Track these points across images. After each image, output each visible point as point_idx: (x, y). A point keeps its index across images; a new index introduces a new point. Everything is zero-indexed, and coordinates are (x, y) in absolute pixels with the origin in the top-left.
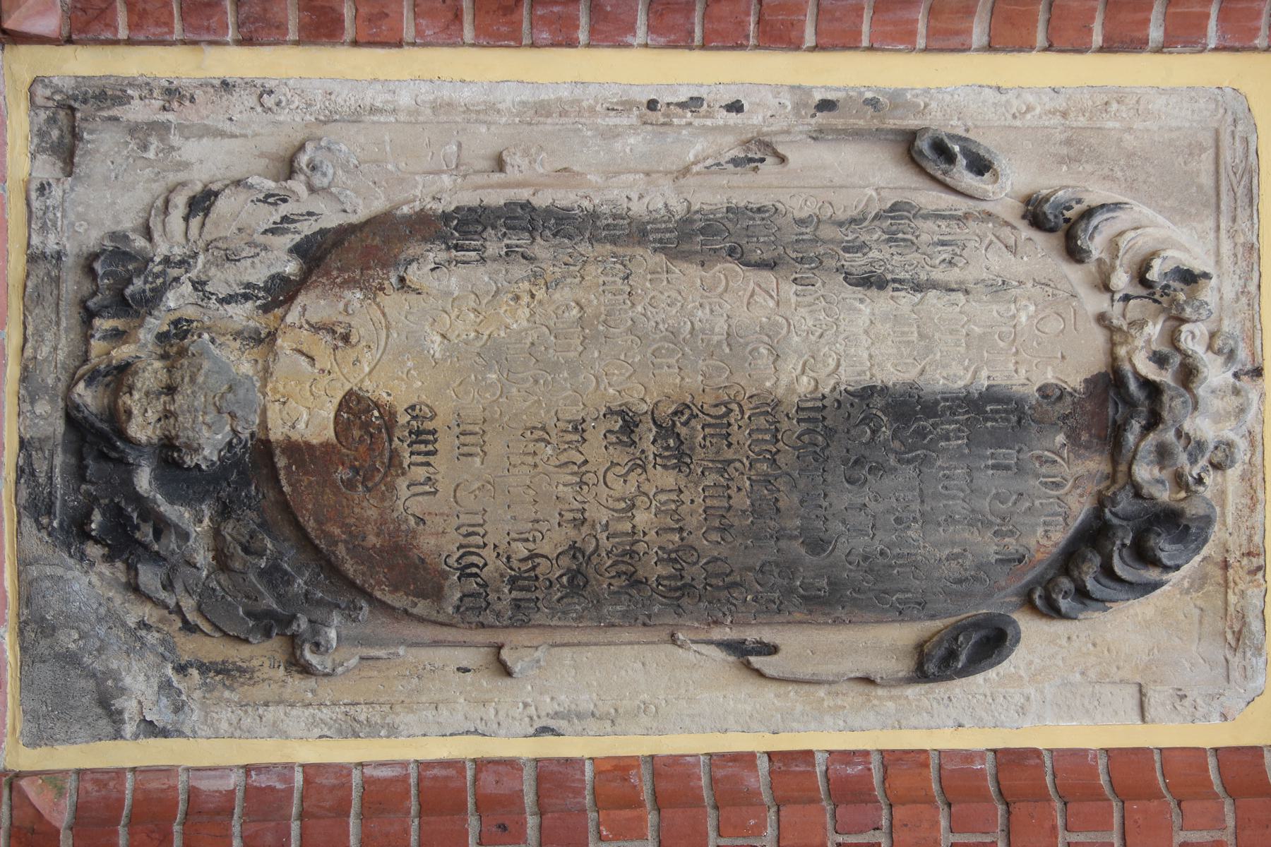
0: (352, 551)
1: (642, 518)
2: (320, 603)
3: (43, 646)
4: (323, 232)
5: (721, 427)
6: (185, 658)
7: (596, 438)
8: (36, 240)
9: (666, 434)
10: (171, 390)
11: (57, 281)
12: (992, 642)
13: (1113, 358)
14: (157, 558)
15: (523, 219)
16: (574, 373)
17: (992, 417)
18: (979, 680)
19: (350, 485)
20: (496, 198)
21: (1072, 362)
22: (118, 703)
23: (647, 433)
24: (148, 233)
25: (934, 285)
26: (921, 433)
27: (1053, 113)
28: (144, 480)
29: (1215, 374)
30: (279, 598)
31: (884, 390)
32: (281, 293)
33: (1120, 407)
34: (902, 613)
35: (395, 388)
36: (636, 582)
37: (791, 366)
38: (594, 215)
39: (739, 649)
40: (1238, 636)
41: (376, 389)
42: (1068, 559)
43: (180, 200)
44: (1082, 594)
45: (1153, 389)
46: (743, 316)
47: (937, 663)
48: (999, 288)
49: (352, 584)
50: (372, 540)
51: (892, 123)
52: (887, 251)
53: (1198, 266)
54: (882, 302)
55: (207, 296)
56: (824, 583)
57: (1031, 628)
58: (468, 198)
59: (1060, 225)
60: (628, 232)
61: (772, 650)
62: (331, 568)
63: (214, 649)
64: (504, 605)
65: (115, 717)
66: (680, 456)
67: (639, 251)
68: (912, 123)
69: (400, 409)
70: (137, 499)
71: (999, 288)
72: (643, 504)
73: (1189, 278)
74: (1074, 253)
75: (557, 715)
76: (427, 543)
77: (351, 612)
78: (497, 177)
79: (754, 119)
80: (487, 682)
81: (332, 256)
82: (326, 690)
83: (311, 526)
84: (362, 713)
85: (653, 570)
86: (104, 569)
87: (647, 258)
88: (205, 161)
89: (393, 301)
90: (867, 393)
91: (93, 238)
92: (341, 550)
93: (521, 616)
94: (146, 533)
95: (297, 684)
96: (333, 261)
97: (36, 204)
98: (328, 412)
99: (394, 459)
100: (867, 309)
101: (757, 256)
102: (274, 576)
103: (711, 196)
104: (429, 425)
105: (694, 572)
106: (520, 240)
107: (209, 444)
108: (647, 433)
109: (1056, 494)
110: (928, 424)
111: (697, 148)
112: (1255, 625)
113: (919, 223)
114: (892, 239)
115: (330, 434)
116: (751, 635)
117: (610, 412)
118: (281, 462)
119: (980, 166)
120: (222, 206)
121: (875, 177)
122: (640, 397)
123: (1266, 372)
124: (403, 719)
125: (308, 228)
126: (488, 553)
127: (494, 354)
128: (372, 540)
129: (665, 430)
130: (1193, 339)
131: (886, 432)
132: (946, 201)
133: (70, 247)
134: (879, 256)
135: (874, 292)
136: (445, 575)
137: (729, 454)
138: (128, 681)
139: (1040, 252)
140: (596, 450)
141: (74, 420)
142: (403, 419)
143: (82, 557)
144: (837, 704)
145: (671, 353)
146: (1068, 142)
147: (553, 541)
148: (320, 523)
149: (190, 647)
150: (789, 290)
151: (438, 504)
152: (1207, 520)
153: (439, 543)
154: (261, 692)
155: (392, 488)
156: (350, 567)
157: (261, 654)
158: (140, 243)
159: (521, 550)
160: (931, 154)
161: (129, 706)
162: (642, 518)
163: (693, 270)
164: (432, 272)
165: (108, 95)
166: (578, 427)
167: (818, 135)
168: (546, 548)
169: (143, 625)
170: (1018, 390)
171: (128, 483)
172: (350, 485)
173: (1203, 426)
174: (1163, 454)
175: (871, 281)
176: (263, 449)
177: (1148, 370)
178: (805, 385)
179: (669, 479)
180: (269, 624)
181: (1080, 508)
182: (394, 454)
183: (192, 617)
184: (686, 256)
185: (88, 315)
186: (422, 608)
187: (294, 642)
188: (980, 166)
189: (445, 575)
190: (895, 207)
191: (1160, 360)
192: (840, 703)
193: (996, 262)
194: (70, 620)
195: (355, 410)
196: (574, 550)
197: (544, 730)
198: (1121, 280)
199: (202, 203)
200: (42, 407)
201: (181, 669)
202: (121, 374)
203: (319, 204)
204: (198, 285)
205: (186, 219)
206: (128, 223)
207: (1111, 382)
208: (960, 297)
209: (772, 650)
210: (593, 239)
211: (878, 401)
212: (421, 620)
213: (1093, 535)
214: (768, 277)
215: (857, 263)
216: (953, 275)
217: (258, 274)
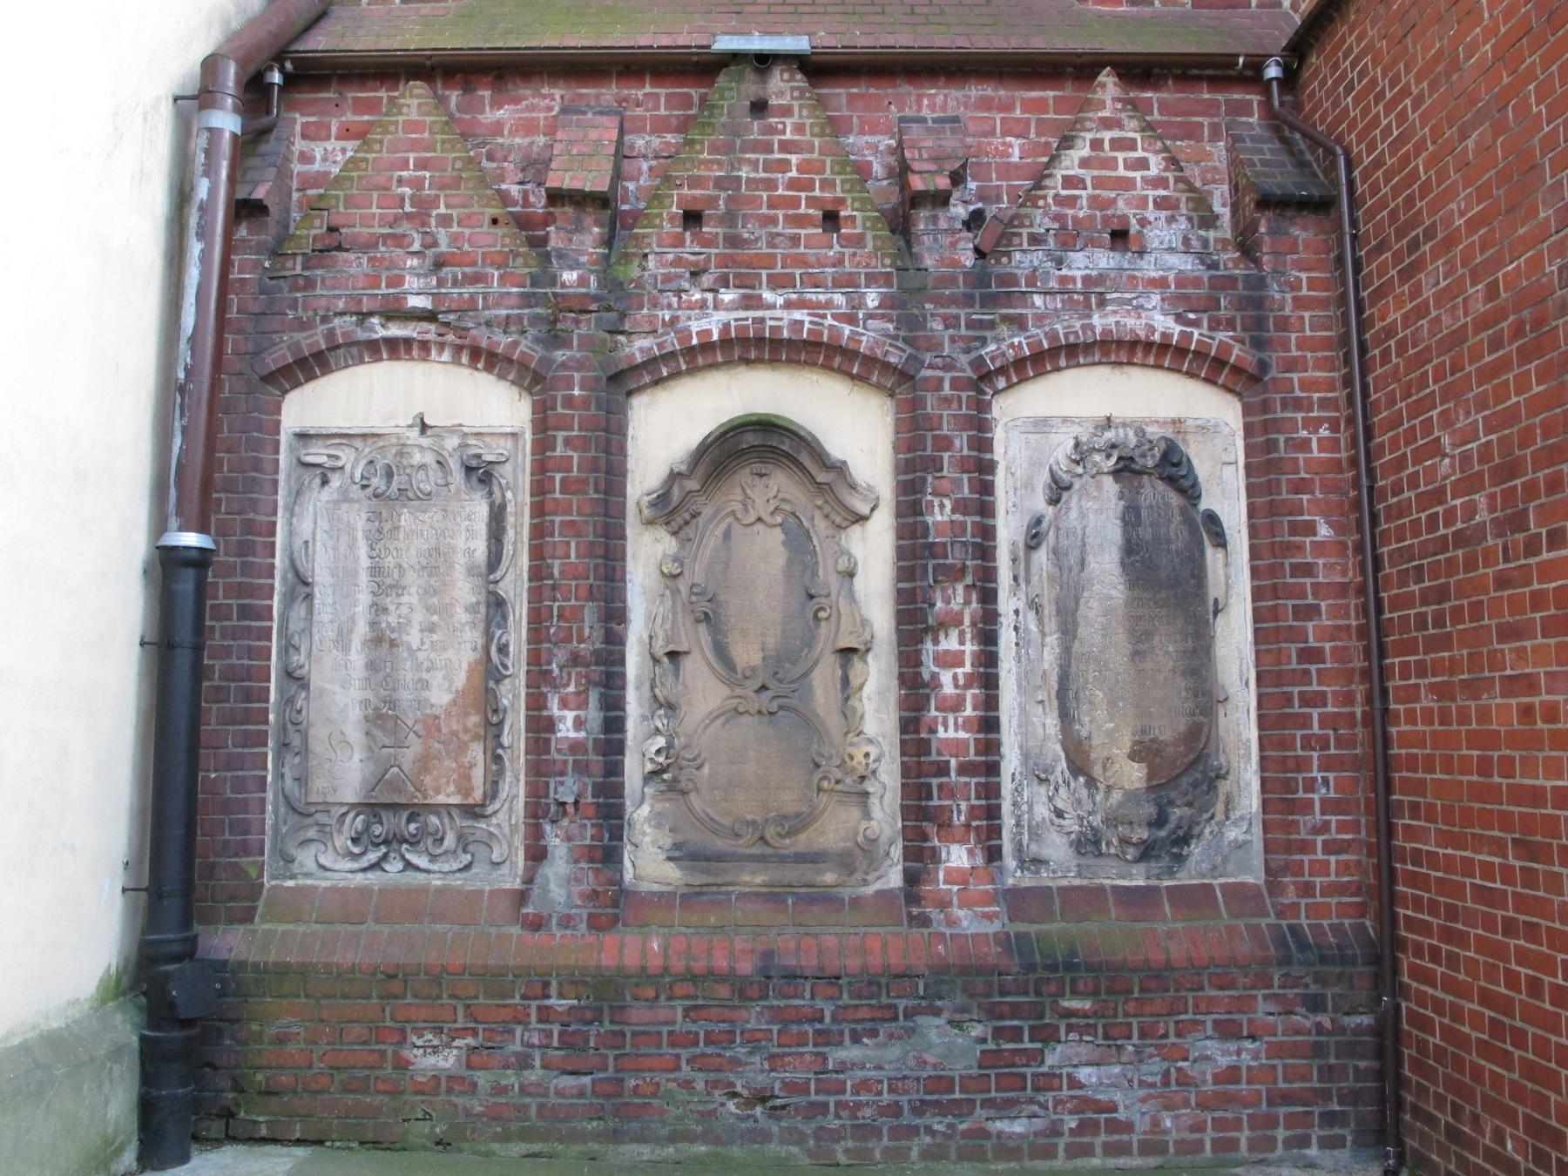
0: (1187, 755)
8: (390, 621)
9: (1140, 639)
10: (1131, 823)
12: (1212, 519)
14: (1190, 828)
15: (1062, 694)
18: (1225, 526)
20: (1055, 704)
21: (1110, 486)
23: (1141, 647)
24: (1070, 833)
28: (1163, 833)
29: (1109, 435)
32: (1091, 783)
33: (1126, 470)
34: (1202, 552)
35: (1126, 741)
36: (1195, 650)
37: (1114, 593)
38: (1061, 666)
39: (1216, 612)
41: (1126, 750)
42: (1182, 491)
43: (1057, 821)
45: (1120, 459)
47: (1220, 540)
51: (1022, 554)
53: (1072, 442)
54: (1090, 558)
58: (1056, 714)
59: (1058, 491)
60: (1066, 650)
61: (1216, 601)
63: (1220, 807)
65: (1246, 842)
66: (1148, 635)
68: (1021, 545)
70: (1168, 837)
72: (1167, 648)
73: (1077, 445)
74: (1068, 488)
76: (1182, 728)
77: (1209, 755)
79: (1021, 605)
80: (1229, 706)
81: (1079, 761)
82: (1234, 765)
88: (1042, 811)
89: (1095, 742)
90: (1123, 564)
91: (1070, 851)
93: (1208, 694)
94: (1181, 833)
95: (1231, 777)
96: (1079, 763)
98: (1136, 765)
99: (1153, 741)
100: (1093, 564)
101: (1073, 604)
102: (1195, 785)
103: (1052, 625)
105: (1191, 629)
106: (1071, 694)
107: (1150, 810)
108: (1141, 647)
109: (1154, 492)
111: (1033, 627)
116: (1211, 608)
119: (1039, 521)
120: (1060, 805)
121: (1042, 557)
122: (1127, 648)
124: (1244, 737)
125: (1067, 774)
127: (1112, 703)
129: (1139, 641)
130: (1100, 442)
134: (1073, 559)
139: (1072, 500)
140: (1149, 665)
144: (1232, 574)
147: (1181, 682)
149: (1219, 816)
150: (1086, 594)
151: (1168, 729)
152: (1166, 439)
156: (1192, 757)
157: (1224, 787)
159: (1184, 694)
160: (1034, 539)
161: (1241, 838)
165: (1019, 848)
166: (1139, 672)
167: (1028, 582)
170: (1120, 508)
173: (1133, 440)
174: (1143, 456)
175: (1083, 563)
176: (1150, 789)
177: (1114, 460)
178: (1121, 587)
179: (1157, 639)
180: (1212, 788)
181: (1161, 486)
184: (1075, 631)
185: (1101, 854)
186: (1206, 730)
187: (1218, 777)
188: (1039, 521)
191: (1108, 456)
192: (847, 330)
193: (1073, 514)
195: (1133, 756)
196: (1184, 674)
198: (1080, 470)
199: (1059, 814)
201: (1227, 818)
202: (1124, 841)
203: (1058, 770)
204: (1090, 814)
206: (1065, 840)
207: (1116, 474)
209: (1216, 601)
213: (1171, 481)
215: (1076, 569)
217: (1084, 793)
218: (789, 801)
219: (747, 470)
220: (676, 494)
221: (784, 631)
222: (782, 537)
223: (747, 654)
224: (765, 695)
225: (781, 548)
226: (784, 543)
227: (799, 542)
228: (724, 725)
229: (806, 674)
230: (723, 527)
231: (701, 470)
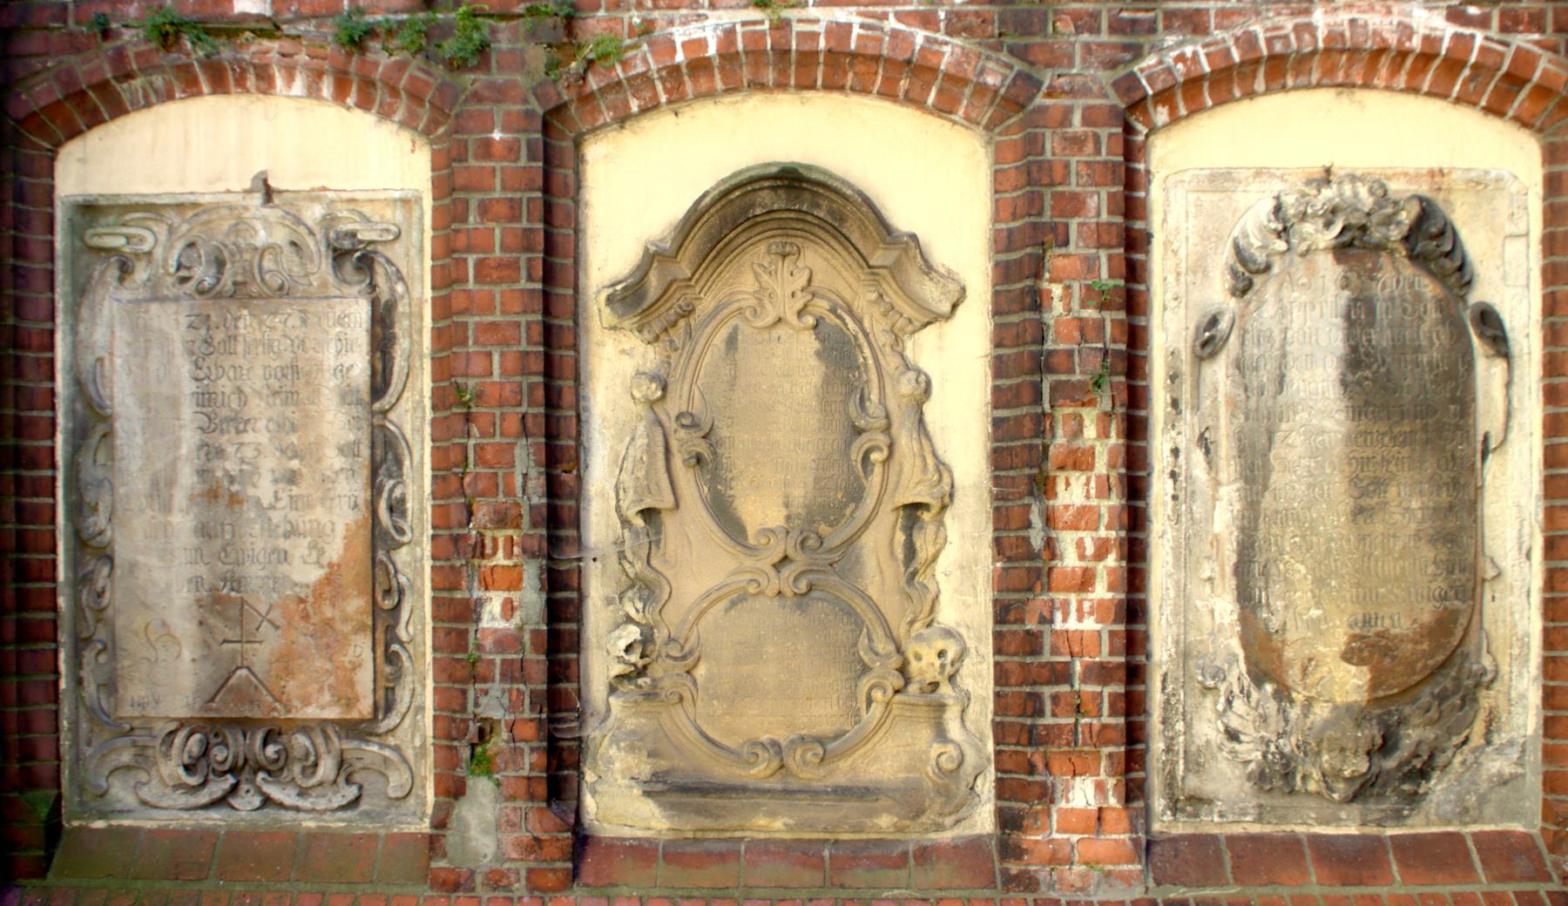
1: (1415, 504)
2: (1459, 672)
3: (1474, 813)
4: (1249, 673)
5: (1364, 462)
6: (1482, 741)
7: (1367, 529)
11: (1273, 808)
12: (1488, 319)
13: (1325, 249)
16: (1332, 539)
17: (1359, 315)
19: (1394, 658)
20: (1232, 582)
22: (1507, 776)
24: (1246, 763)
25: (1283, 346)
26: (1367, 354)
27: (1177, 280)
28: (1390, 763)
30: (1454, 693)
31: (1343, 374)
35: (1340, 636)
37: (1329, 424)
40: (1478, 183)
44: (1461, 268)
46: (1300, 450)
48: (1283, 312)
49: (1450, 657)
50: (1425, 646)
52: (1262, 372)
55: (1285, 732)
56: (1452, 407)
57: (1476, 296)
62: (1443, 665)
64: (1463, 577)
67: (1263, 505)
69: (1351, 632)
70: (1400, 766)
71: (1283, 312)
72: (1409, 503)
75: (1520, 549)
76: (1427, 618)
77: (1466, 656)
78: (1217, 582)
82: (1504, 669)
83: (1417, 678)
84: (1516, 651)
85: (1444, 497)
86: (1433, 782)
87: (1267, 502)
89: (1291, 635)
92: (1431, 662)
97: (1231, 818)
99: (1379, 635)
100: (1297, 380)
103: (1228, 468)
104: (1360, 617)
106: (1256, 569)
109: (1397, 277)
110: (1362, 350)
112: (1473, 175)
113: (1247, 354)
114: (1256, 369)
115: (1365, 669)
116: (1479, 447)
117: (1354, 521)
118: (1381, 693)
119: (1214, 321)
122: (1344, 504)
123: (1435, 164)
124: (1519, 631)
125: (1246, 681)
126: (1434, 586)
127: (1320, 582)
128: (1425, 646)
131: (1368, 373)
132: (1233, 339)
133: (1254, 802)
134: (1265, 376)
135: (1287, 379)
136: (1446, 609)
137: (1379, 458)
138: (1494, 770)
141: (1353, 798)
142: (1357, 631)
143: (1426, 794)
145: (1322, 488)
146: (1195, 272)
147: (1427, 553)
148: (1415, 673)
149: (1477, 740)
150: (1284, 426)
153: (1427, 614)
154: (1502, 700)
155: (1396, 636)
156: (1440, 658)
157: (1486, 700)
158: (1252, 766)
159: (1431, 569)
160: (1208, 344)
162: (1415, 504)
163: (1274, 477)
164: (1275, 614)
166: (1362, 538)
168: (1431, 555)
169: (1463, 763)
171: (1388, 772)
172: (1394, 658)
175: (1281, 381)
179: (1393, 490)
182: (1378, 635)
183: (1462, 738)
184: (1266, 479)
185: (1292, 792)
186: (1463, 621)
188: (1214, 321)
189: (1446, 609)
190: (1238, 367)
193: (1269, 310)
194: (1460, 799)
195: (1349, 656)
197: (1528, 556)
199: (1233, 735)
200: (1343, 815)
201: (1489, 743)
204: (1280, 736)
205: (1240, 742)
208: (1290, 334)
210: (1256, 529)
211: (1350, 378)
212: (1470, 621)
214: (1278, 436)
215: (1271, 389)
216: (1277, 337)
217: (1272, 706)
218: (823, 715)
219: (763, 247)
220: (654, 283)
221: (817, 480)
222: (817, 345)
223: (762, 511)
224: (788, 572)
225: (814, 362)
226: (818, 354)
227: (840, 352)
228: (727, 610)
229: (851, 541)
230: (724, 333)
231: (691, 249)
